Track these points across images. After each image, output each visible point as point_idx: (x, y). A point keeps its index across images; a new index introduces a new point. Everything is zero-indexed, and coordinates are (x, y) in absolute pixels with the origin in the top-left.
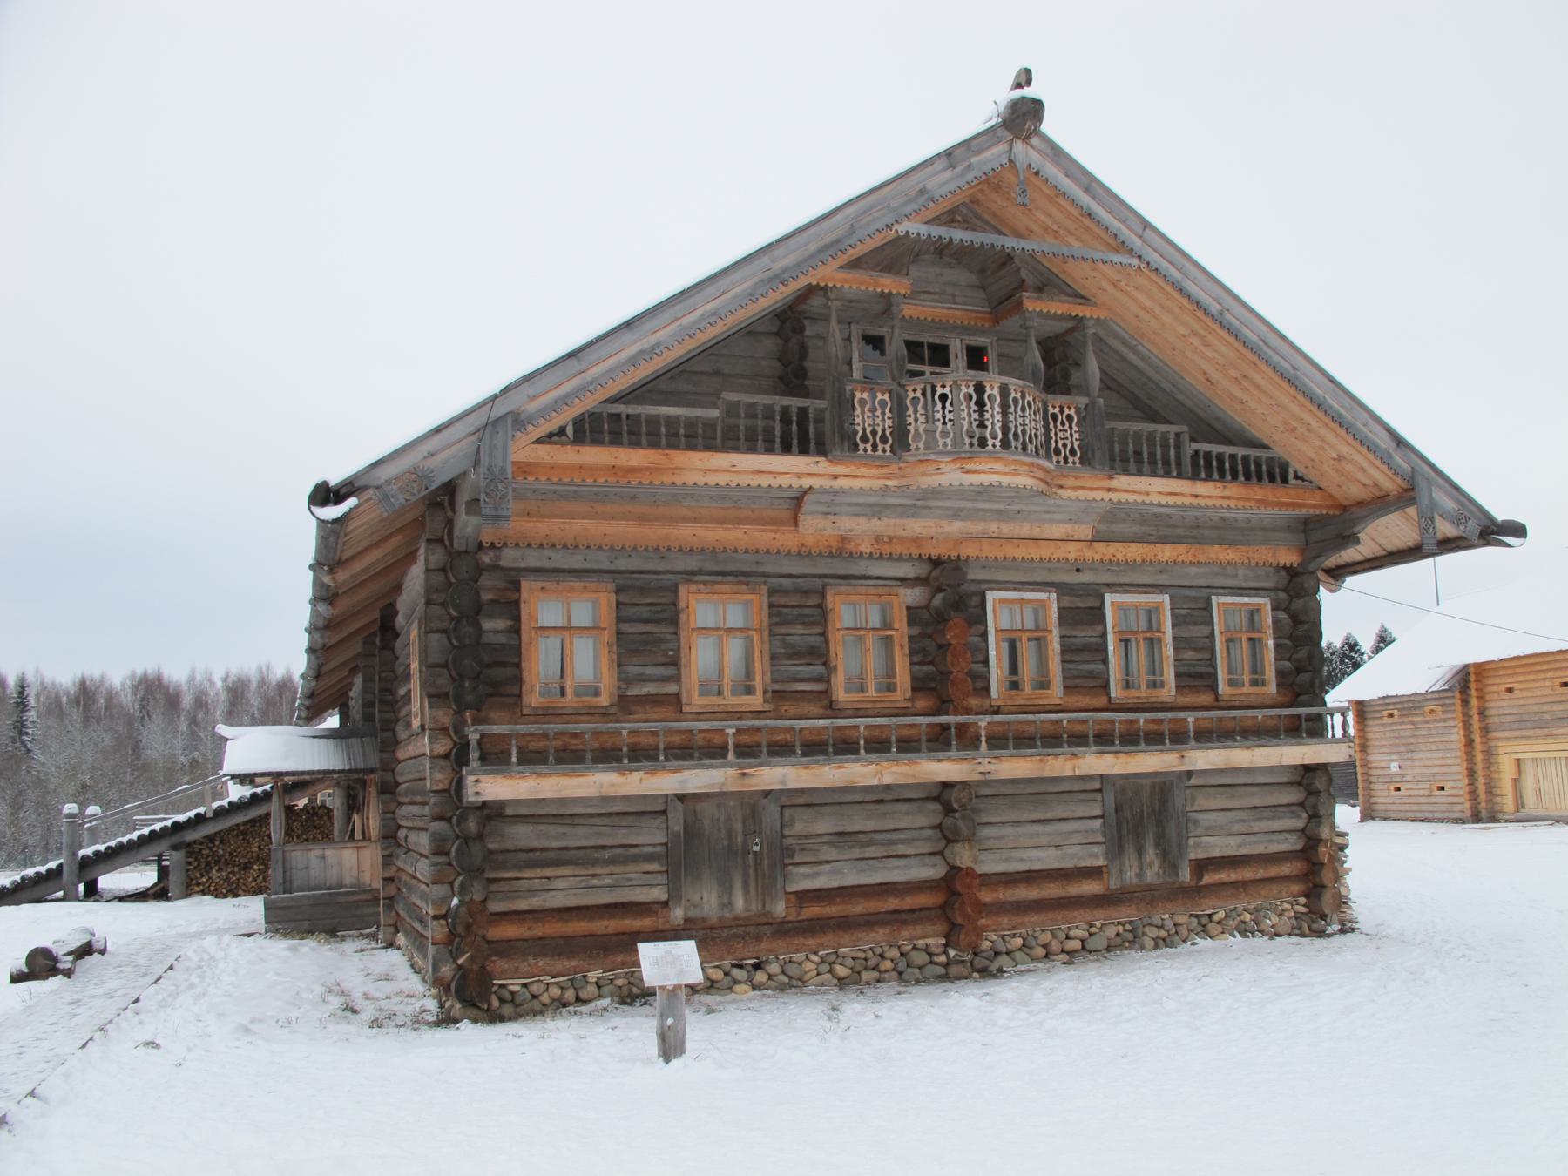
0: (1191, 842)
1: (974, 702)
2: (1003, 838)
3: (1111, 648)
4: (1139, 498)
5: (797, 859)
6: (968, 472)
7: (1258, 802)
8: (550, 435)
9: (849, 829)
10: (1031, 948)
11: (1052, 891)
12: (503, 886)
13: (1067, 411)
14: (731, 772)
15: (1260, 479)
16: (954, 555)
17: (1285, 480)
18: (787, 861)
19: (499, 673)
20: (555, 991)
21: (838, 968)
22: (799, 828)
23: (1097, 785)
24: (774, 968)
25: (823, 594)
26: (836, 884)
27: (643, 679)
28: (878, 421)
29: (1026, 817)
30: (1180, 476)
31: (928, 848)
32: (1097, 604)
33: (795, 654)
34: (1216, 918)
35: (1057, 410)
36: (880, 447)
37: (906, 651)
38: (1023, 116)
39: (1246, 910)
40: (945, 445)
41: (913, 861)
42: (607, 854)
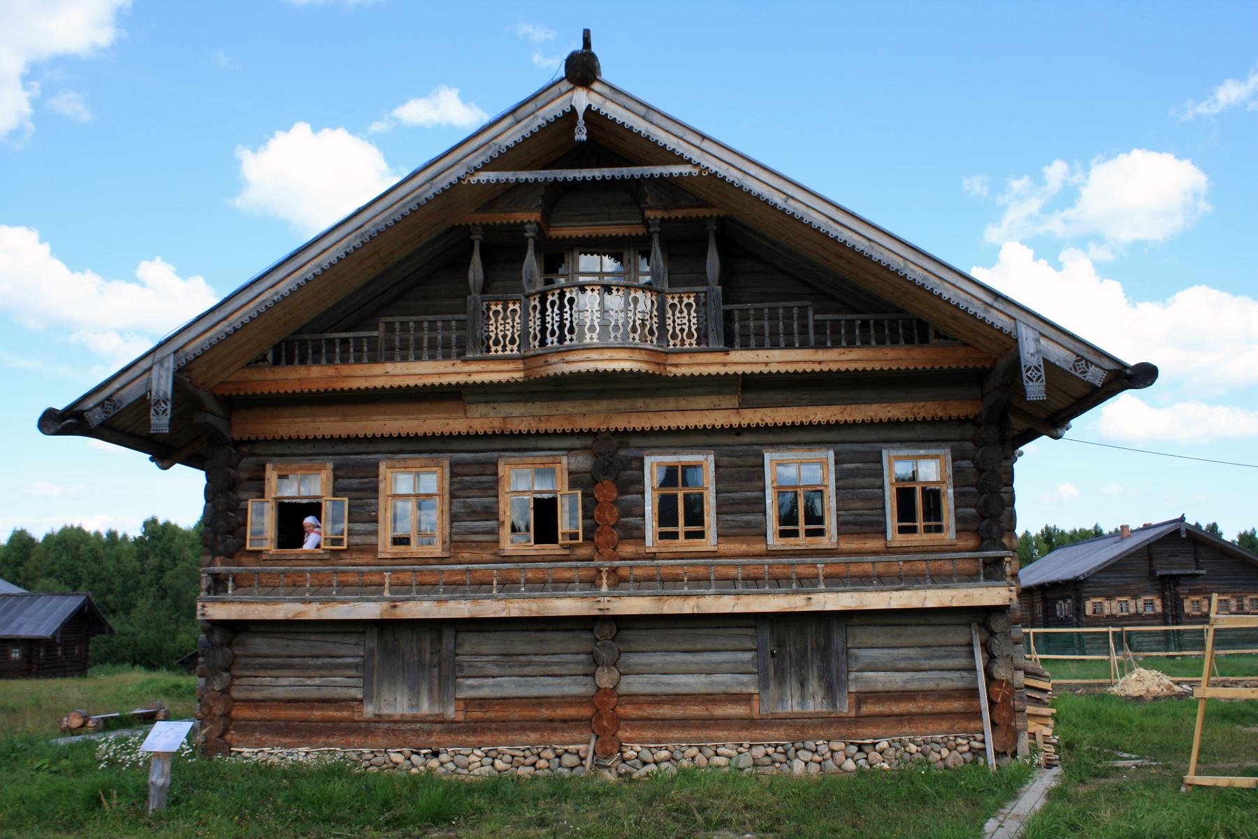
0: (852, 675)
1: (627, 549)
2: (652, 664)
3: (768, 501)
4: (757, 369)
5: (466, 672)
6: (568, 362)
7: (929, 640)
9: (511, 651)
11: (697, 711)
12: (244, 681)
13: (686, 300)
14: (385, 605)
16: (603, 427)
18: (459, 674)
21: (497, 762)
22: (467, 648)
24: (443, 757)
25: (496, 465)
26: (498, 695)
28: (508, 327)
29: (674, 647)
30: (804, 345)
31: (580, 669)
32: (759, 461)
33: (474, 514)
34: (877, 747)
35: (676, 301)
36: (687, 342)
38: (582, 69)
39: (913, 742)
40: (592, 338)
41: (568, 680)
42: (319, 661)
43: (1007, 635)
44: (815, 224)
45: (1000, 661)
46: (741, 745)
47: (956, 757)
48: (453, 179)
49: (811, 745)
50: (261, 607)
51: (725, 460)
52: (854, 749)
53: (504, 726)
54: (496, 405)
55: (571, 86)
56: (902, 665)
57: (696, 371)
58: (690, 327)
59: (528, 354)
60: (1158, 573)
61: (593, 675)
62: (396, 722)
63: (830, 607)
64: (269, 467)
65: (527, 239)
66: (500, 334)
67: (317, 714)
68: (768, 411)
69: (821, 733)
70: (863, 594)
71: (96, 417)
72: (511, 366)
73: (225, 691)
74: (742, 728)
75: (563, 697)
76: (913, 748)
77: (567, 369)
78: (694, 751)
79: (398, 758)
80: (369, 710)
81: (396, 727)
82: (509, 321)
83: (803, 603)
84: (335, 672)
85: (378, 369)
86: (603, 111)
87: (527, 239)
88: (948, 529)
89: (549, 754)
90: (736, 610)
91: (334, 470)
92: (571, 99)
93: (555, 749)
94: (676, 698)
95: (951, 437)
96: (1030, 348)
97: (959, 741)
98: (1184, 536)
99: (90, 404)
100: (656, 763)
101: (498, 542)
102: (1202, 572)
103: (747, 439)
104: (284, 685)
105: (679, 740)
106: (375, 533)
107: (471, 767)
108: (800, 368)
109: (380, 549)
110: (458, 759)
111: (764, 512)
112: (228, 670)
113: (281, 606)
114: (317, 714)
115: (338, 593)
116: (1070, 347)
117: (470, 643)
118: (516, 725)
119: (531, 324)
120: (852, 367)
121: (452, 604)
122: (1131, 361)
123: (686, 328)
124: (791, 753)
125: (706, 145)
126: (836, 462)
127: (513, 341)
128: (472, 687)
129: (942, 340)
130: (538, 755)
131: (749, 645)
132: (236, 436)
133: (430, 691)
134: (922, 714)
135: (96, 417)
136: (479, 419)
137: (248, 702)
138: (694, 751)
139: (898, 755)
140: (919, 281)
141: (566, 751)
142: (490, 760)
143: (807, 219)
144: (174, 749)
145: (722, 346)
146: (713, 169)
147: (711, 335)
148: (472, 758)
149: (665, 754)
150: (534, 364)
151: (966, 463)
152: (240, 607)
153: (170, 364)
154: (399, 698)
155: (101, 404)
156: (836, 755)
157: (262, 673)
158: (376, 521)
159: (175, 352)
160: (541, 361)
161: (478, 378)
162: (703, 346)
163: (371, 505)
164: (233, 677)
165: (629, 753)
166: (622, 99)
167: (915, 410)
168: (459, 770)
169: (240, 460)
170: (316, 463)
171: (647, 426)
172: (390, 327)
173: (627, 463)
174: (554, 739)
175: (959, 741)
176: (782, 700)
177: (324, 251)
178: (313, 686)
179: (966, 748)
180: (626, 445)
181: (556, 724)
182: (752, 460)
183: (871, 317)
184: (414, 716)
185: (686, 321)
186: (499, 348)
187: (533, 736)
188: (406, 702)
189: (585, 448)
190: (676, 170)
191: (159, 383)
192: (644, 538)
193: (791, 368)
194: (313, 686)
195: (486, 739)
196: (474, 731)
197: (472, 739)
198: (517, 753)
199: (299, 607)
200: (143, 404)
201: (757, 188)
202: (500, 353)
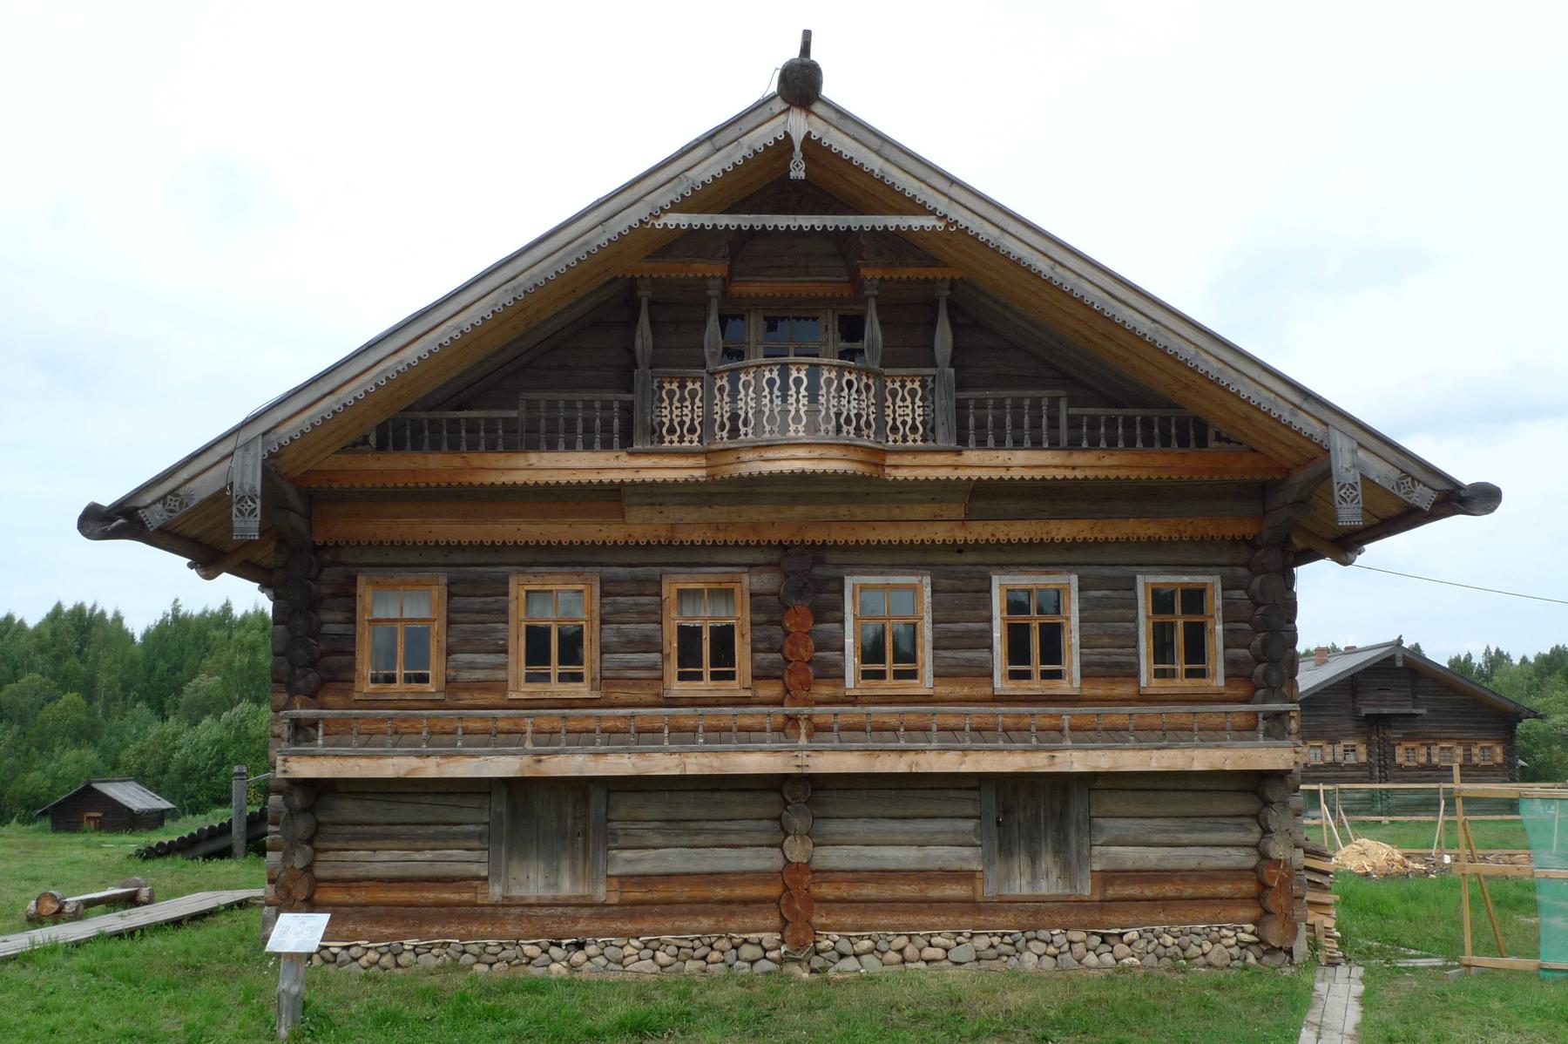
0: (1096, 850)
1: (824, 691)
2: (852, 833)
4: (995, 474)
5: (621, 842)
7: (1189, 809)
8: (355, 445)
10: (883, 953)
11: (908, 890)
12: (331, 855)
13: (909, 385)
14: (527, 759)
15: (1166, 443)
16: (797, 539)
17: (1202, 442)
19: (335, 661)
20: (372, 955)
21: (659, 954)
22: (623, 812)
23: (975, 784)
24: (591, 950)
25: (660, 583)
26: (661, 870)
27: (472, 667)
28: (686, 411)
30: (1054, 445)
31: (764, 839)
33: (631, 645)
34: (1125, 938)
35: (897, 385)
36: (911, 437)
37: (748, 638)
38: (800, 83)
40: (797, 431)
41: (749, 852)
42: (431, 830)
43: (1285, 804)
44: (1088, 299)
45: (1277, 837)
46: (960, 934)
47: (1220, 952)
48: (634, 222)
49: (1044, 934)
50: (363, 762)
51: (944, 583)
52: (1096, 940)
53: (668, 907)
54: (663, 508)
55: (785, 106)
56: (1156, 838)
57: (922, 474)
58: (914, 419)
59: (714, 447)
60: (1365, 711)
61: (780, 846)
62: (530, 905)
63: (1078, 767)
64: (361, 579)
65: (709, 298)
66: (676, 420)
67: (430, 896)
68: (1000, 524)
69: (1058, 920)
70: (1117, 753)
71: (155, 518)
72: (691, 462)
73: (308, 868)
74: (963, 913)
75: (744, 873)
76: (1169, 940)
77: (766, 468)
78: (903, 941)
79: (531, 950)
80: (496, 892)
81: (533, 911)
82: (687, 403)
83: (1046, 762)
84: (451, 844)
85: (520, 460)
86: (826, 141)
87: (709, 298)
88: (1215, 675)
89: (723, 944)
90: (963, 769)
91: (448, 585)
92: (785, 123)
93: (731, 939)
94: (883, 875)
95: (1223, 560)
96: (1345, 460)
97: (1224, 932)
98: (1400, 664)
99: (148, 498)
100: (857, 955)
101: (662, 679)
102: (1420, 711)
103: (971, 557)
104: (385, 860)
105: (886, 928)
106: (504, 666)
107: (626, 962)
108: (1049, 474)
109: (511, 685)
110: (609, 951)
111: (991, 648)
112: (310, 841)
113: (390, 761)
114: (430, 896)
115: (464, 745)
116: (1393, 460)
117: (625, 807)
118: (685, 908)
119: (717, 409)
120: (1112, 474)
121: (612, 758)
122: (1466, 477)
123: (909, 420)
124: (1020, 945)
125: (955, 192)
126: (1081, 589)
127: (692, 430)
128: (629, 861)
129: (1224, 444)
130: (711, 946)
131: (971, 811)
132: (319, 541)
133: (573, 868)
134: (1180, 899)
135: (155, 518)
136: (640, 525)
137: (334, 881)
138: (903, 941)
139: (1150, 948)
140: (1214, 374)
141: (746, 941)
142: (650, 952)
143: (1078, 293)
144: (314, 948)
145: (953, 445)
146: (963, 223)
147: (940, 431)
148: (628, 950)
149: (867, 944)
150: (724, 461)
151: (1237, 594)
152: (335, 761)
153: (258, 451)
154: (532, 876)
155: (163, 499)
156: (1074, 947)
157: (354, 845)
158: (506, 652)
159: (264, 434)
160: (732, 458)
161: (648, 476)
162: (931, 444)
163: (498, 631)
164: (316, 851)
165: (825, 944)
166: (851, 128)
167: (1181, 528)
168: (611, 966)
169: (321, 570)
170: (425, 575)
171: (852, 539)
172: (533, 405)
173: (821, 585)
174: (731, 925)
175: (1224, 932)
176: (1008, 878)
177: (465, 308)
178: (422, 860)
179: (1233, 941)
180: (820, 561)
181: (734, 907)
182: (976, 584)
183: (1138, 414)
184: (554, 898)
185: (909, 411)
186: (675, 438)
187: (706, 923)
188: (541, 882)
189: (769, 564)
190: (916, 222)
191: (243, 475)
192: (843, 677)
193: (1038, 474)
194: (422, 860)
195: (645, 926)
196: (631, 917)
197: (629, 927)
198: (684, 943)
199: (415, 762)
200: (220, 501)
201: (1017, 250)
202: (676, 444)
